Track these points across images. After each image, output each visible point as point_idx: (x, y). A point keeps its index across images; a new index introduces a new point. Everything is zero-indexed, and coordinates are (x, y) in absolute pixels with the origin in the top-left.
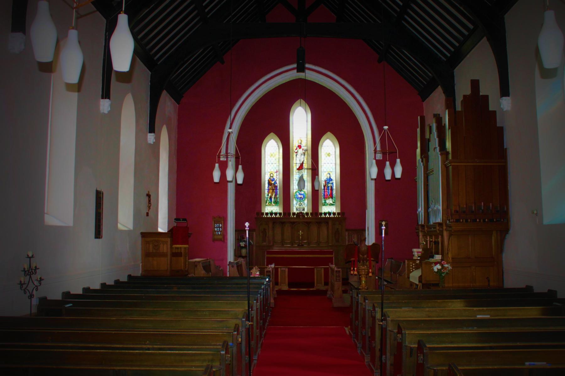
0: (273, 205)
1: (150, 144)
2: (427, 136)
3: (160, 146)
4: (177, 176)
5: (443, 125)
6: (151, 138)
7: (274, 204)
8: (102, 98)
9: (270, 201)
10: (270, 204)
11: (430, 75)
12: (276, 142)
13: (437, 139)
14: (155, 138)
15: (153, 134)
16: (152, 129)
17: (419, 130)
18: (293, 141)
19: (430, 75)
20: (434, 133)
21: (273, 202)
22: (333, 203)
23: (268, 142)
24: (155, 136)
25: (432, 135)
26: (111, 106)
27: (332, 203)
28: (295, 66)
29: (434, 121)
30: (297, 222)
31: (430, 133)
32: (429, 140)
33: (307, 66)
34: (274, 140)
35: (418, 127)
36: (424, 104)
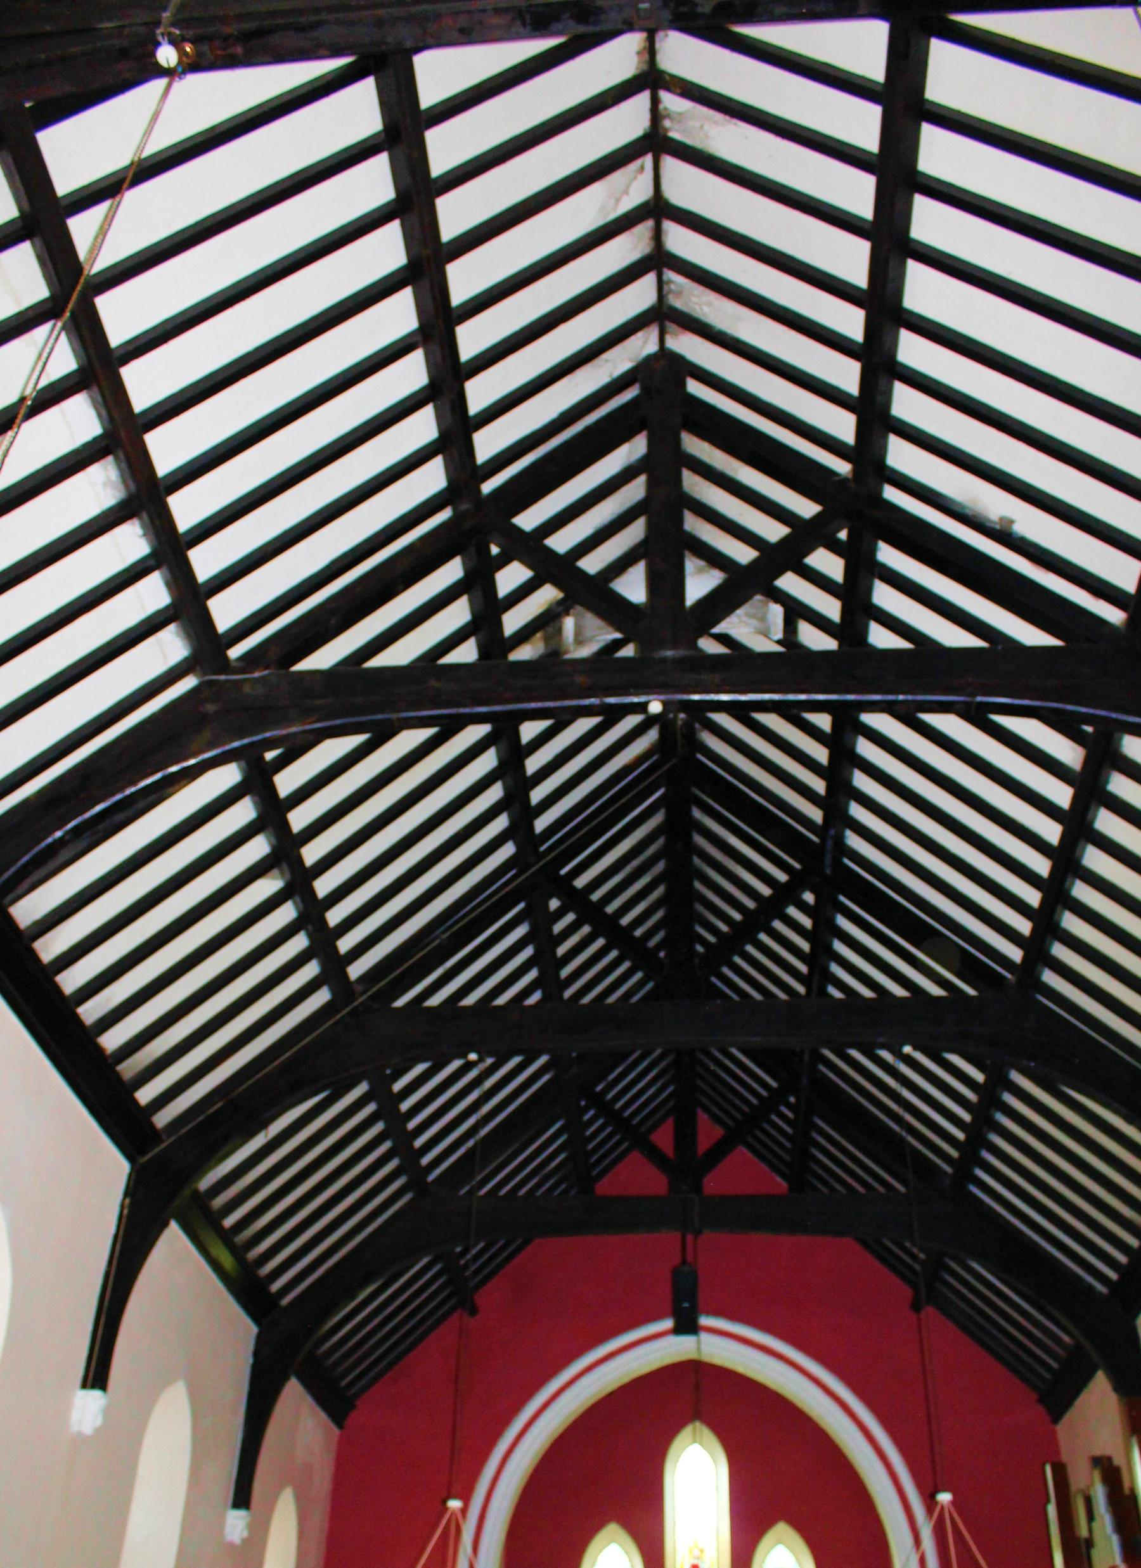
1: (231, 1545)
2: (1083, 1532)
3: (138, 1445)
4: (712, 693)
5: (1127, 1491)
6: (236, 1523)
8: (84, 1385)
11: (1066, 1339)
12: (626, 1552)
13: (1115, 1540)
14: (251, 1527)
15: (242, 1513)
16: (242, 1498)
17: (1052, 1510)
18: (675, 1549)
19: (1066, 1339)
20: (1102, 1517)
23: (601, 1551)
24: (248, 1520)
25: (1096, 1525)
26: (107, 1412)
28: (668, 1324)
29: (1097, 1476)
31: (1091, 1517)
32: (1089, 1543)
33: (705, 1321)
34: (619, 1544)
35: (1048, 1501)
36: (1060, 1428)
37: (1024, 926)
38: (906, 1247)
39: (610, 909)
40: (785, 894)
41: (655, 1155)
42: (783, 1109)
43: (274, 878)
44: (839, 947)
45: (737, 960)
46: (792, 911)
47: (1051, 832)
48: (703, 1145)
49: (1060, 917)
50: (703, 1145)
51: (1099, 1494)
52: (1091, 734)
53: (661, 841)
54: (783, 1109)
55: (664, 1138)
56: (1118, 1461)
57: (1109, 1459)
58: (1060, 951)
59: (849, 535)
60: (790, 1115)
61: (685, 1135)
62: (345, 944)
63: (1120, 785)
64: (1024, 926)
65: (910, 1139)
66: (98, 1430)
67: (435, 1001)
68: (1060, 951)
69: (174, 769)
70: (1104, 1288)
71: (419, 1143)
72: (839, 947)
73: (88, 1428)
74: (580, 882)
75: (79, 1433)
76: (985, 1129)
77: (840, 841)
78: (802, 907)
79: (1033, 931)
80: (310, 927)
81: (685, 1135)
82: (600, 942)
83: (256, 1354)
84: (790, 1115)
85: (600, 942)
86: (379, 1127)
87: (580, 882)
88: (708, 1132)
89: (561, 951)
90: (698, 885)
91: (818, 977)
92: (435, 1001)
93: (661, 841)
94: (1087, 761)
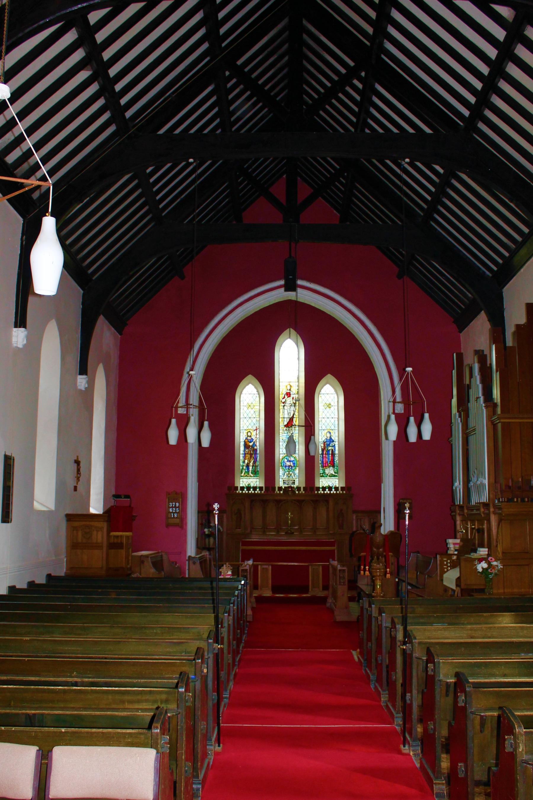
0: (251, 476)
1: (81, 390)
6: (82, 381)
7: (252, 475)
8: (16, 326)
9: (246, 470)
10: (246, 474)
11: (470, 295)
16: (83, 371)
17: (454, 372)
19: (470, 295)
20: (476, 377)
21: (250, 472)
22: (335, 473)
24: (87, 379)
25: (472, 380)
26: (28, 337)
27: (334, 473)
30: (284, 500)
32: (469, 387)
37: (485, 70)
38: (220, 719)
40: (352, 73)
42: (356, 82)
43: (88, 70)
44: (392, 30)
47: (492, 53)
49: (491, 97)
51: (476, 367)
53: (287, 33)
54: (356, 82)
56: (486, 352)
57: (483, 351)
58: (504, 86)
60: (360, 86)
62: (113, 72)
63: (521, 51)
64: (485, 70)
65: (405, 199)
66: (25, 346)
68: (504, 86)
69: (41, 22)
71: (123, 101)
72: (392, 30)
73: (20, 346)
75: (17, 347)
76: (441, 196)
77: (381, 44)
79: (476, 102)
80: (107, 95)
83: (83, 304)
86: (101, 102)
89: (222, 31)
90: (306, 75)
91: (361, 124)
93: (287, 33)
94: (516, 18)
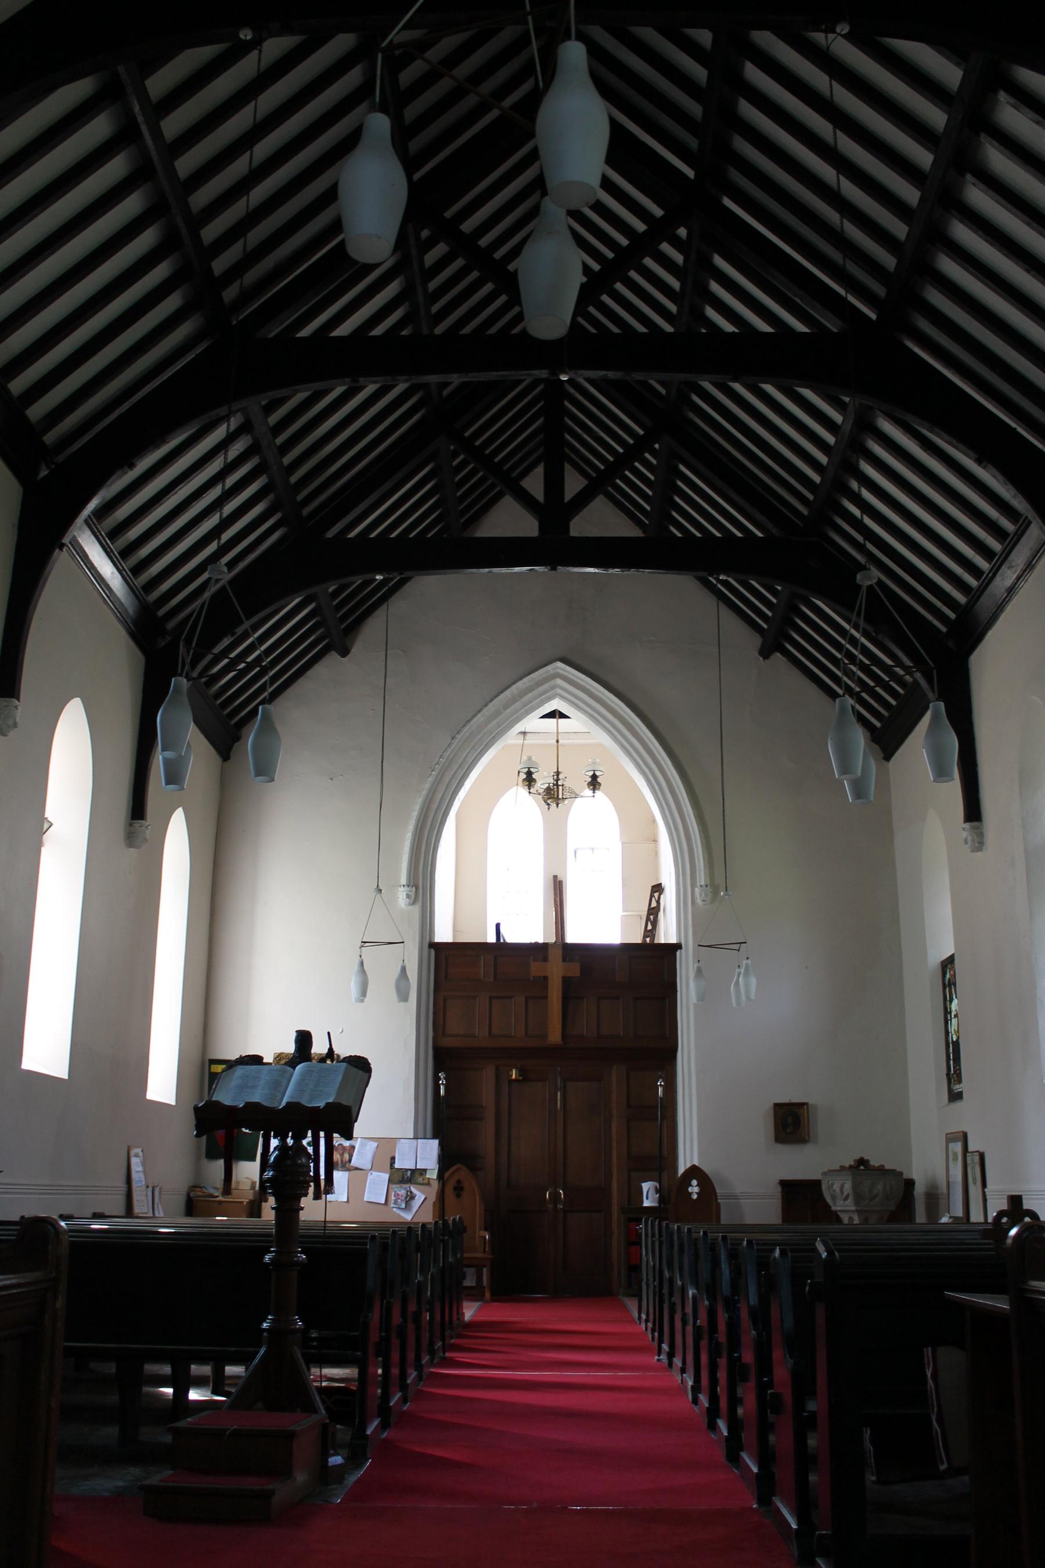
39: (484, 242)
41: (526, 499)
45: (605, 298)
46: (665, 247)
48: (569, 494)
50: (569, 494)
52: (647, 452)
55: (535, 484)
59: (655, 448)
60: (679, 258)
61: (554, 483)
67: (343, 330)
70: (892, 649)
74: (468, 226)
78: (677, 243)
81: (554, 483)
82: (459, 263)
84: (679, 258)
85: (459, 263)
87: (468, 226)
88: (573, 484)
92: (343, 330)
